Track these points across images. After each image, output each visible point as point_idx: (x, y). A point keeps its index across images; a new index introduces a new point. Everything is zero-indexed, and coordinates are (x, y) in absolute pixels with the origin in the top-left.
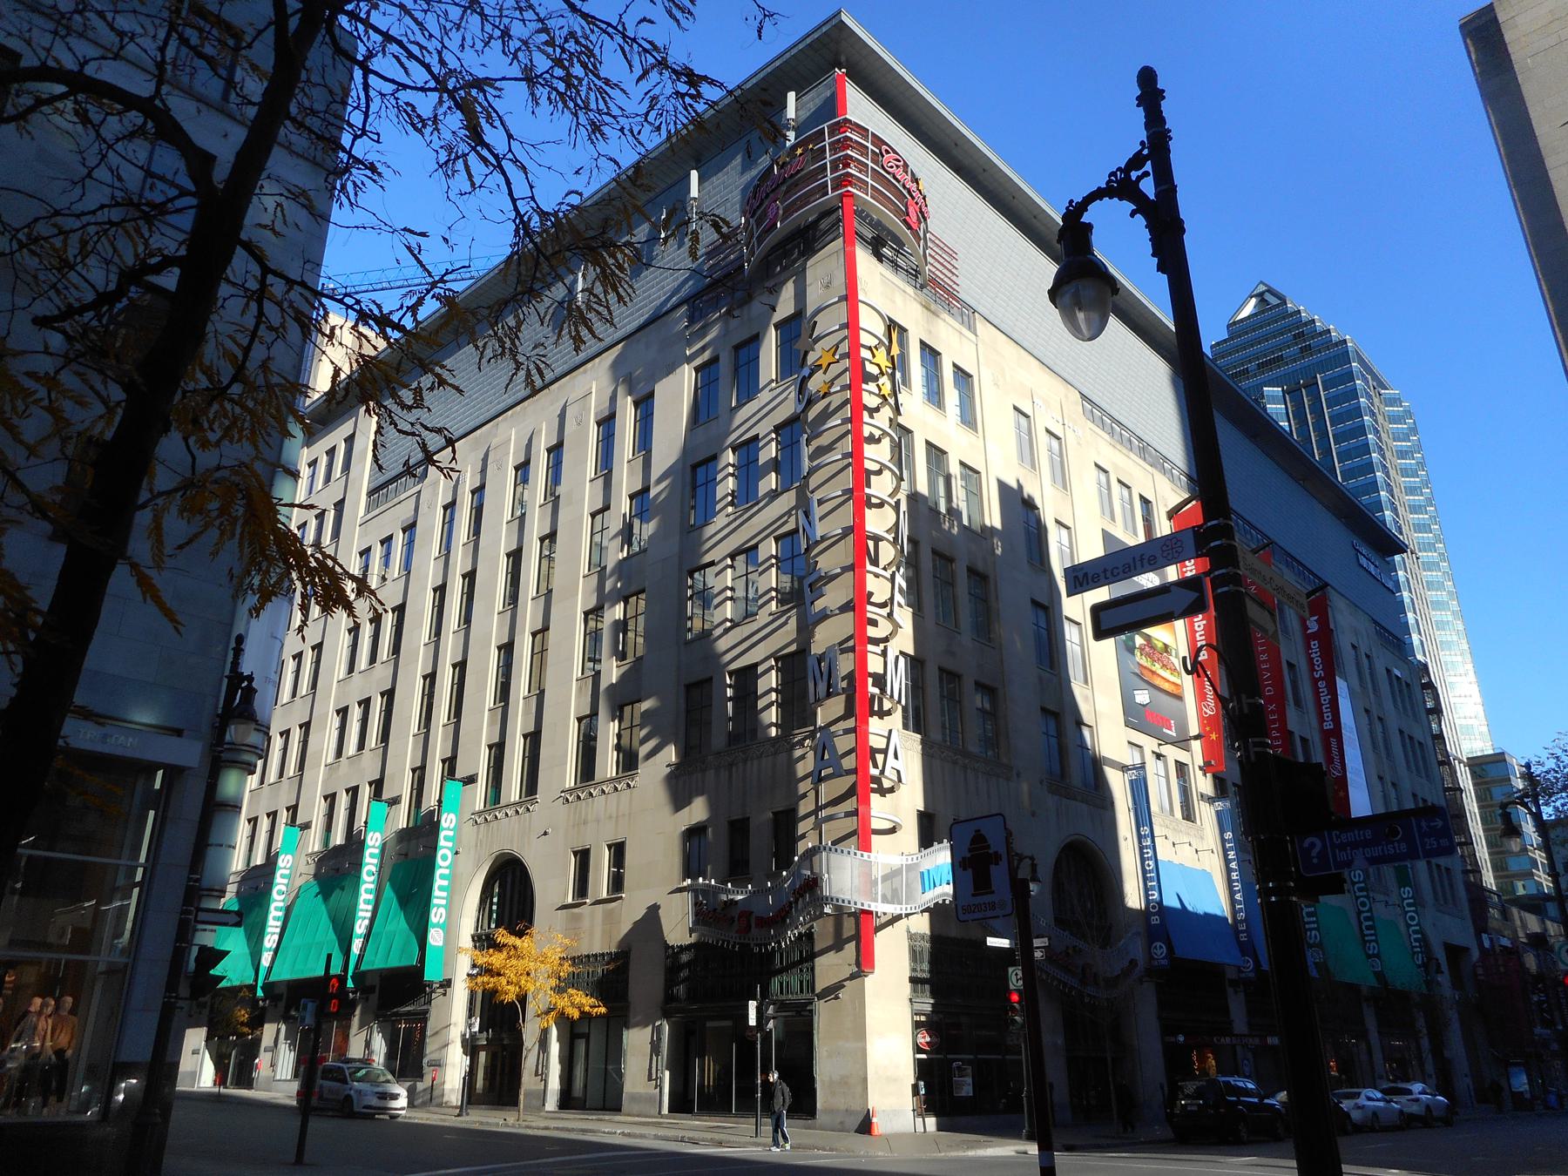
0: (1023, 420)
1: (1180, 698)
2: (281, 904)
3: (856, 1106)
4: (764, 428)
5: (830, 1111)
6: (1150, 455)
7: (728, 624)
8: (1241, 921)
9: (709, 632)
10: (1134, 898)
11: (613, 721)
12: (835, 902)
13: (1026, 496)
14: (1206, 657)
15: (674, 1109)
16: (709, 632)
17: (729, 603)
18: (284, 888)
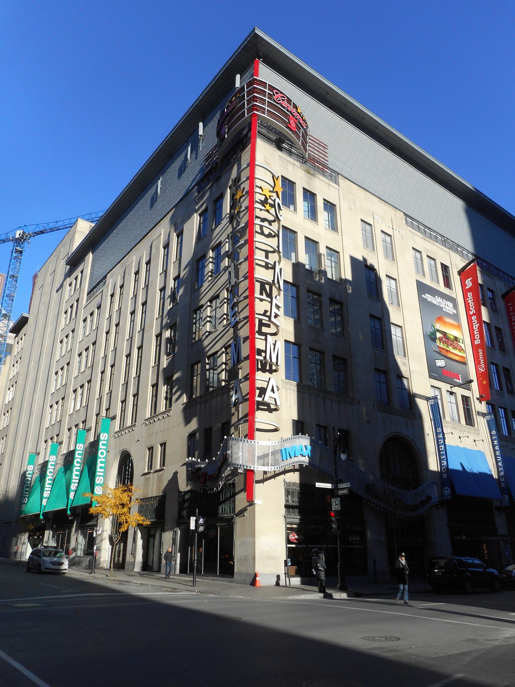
0: (368, 227)
1: (465, 364)
2: (51, 478)
3: (251, 572)
4: (222, 238)
5: (240, 574)
6: (449, 244)
7: (207, 333)
8: (502, 477)
9: (201, 339)
10: (433, 465)
11: (164, 386)
12: (234, 466)
13: (368, 264)
15: (181, 572)
16: (201, 339)
17: (208, 323)
18: (52, 471)
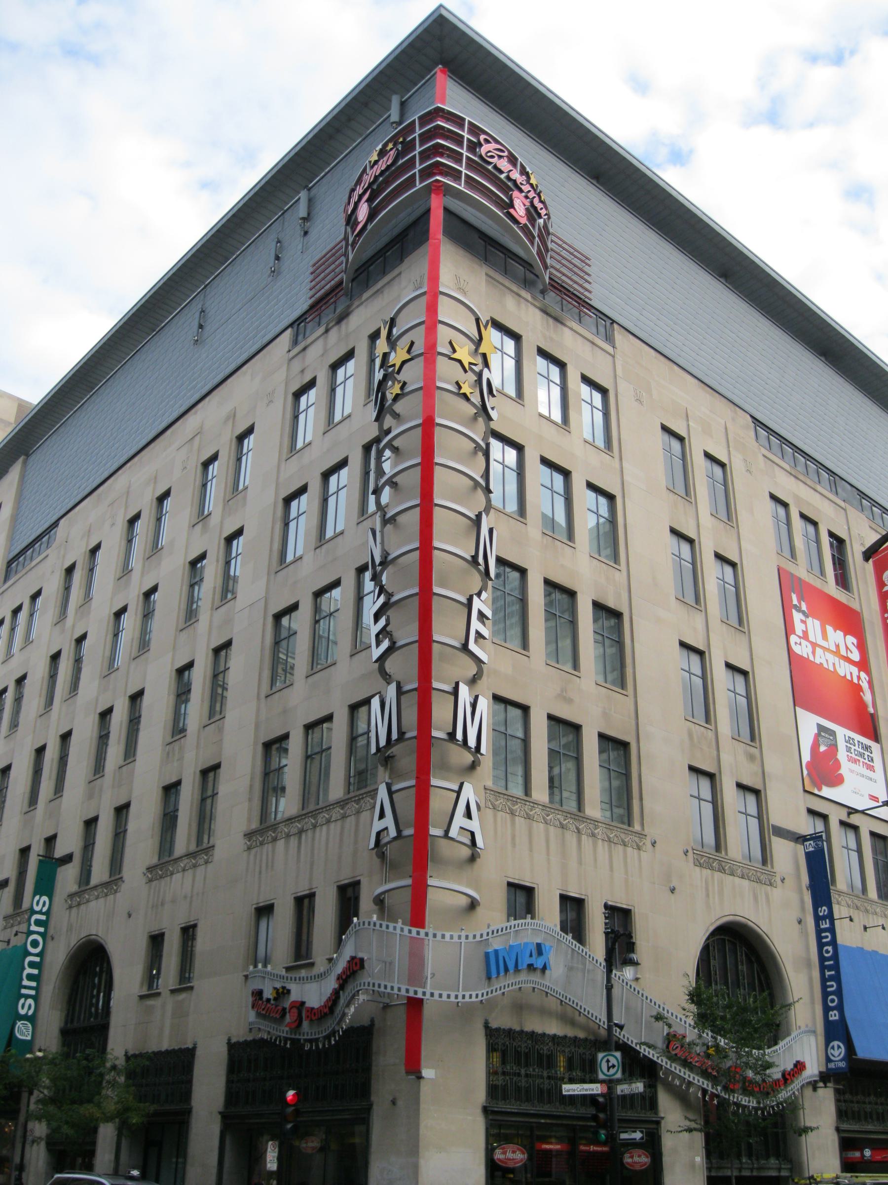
14: (837, 1018)
